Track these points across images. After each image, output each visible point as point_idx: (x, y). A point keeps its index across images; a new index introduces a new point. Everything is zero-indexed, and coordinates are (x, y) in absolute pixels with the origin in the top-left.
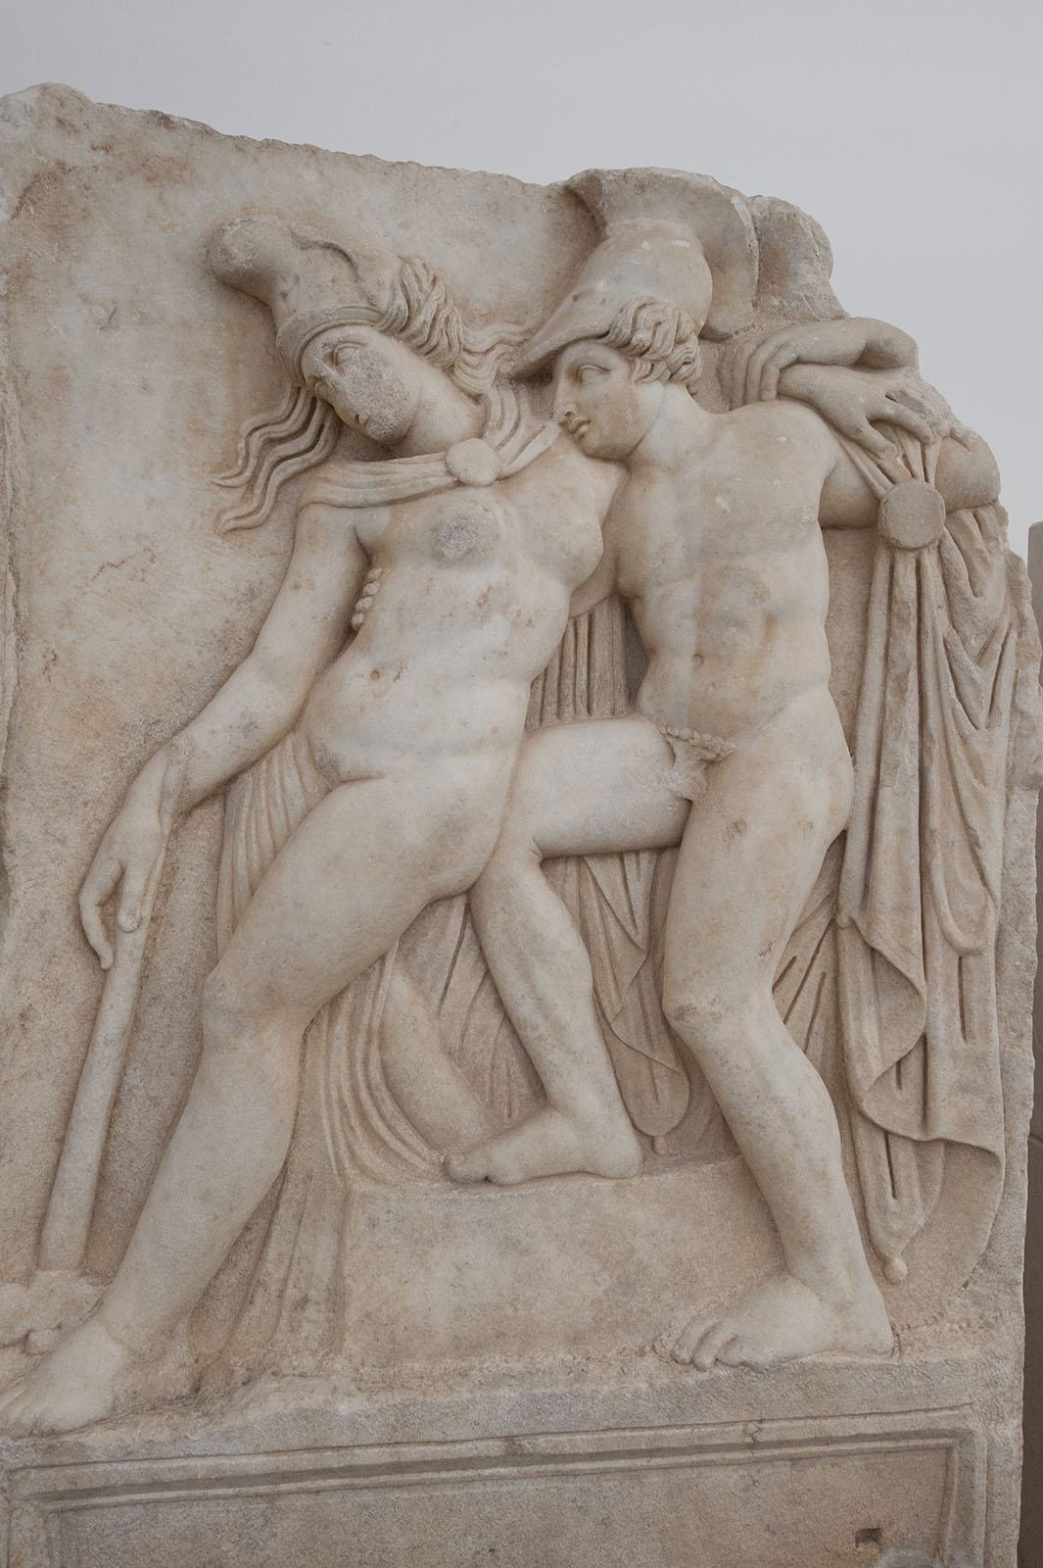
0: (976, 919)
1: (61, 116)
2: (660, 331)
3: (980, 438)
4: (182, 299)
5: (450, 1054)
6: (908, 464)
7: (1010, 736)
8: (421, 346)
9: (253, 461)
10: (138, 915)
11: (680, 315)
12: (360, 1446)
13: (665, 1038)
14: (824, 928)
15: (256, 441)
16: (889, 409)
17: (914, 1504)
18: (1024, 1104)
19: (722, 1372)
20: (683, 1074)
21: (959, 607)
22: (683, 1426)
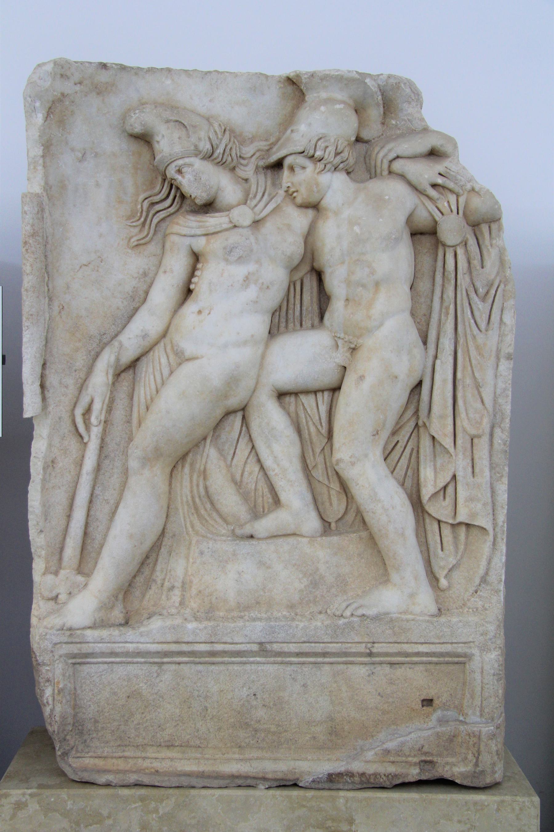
0: (479, 421)
1: (62, 73)
2: (328, 151)
3: (488, 190)
4: (113, 144)
5: (236, 483)
8: (219, 162)
9: (144, 214)
11: (338, 140)
13: (335, 477)
14: (413, 427)
15: (146, 204)
17: (449, 689)
18: (502, 507)
19: (355, 619)
20: (343, 493)
21: (474, 273)
22: (337, 643)
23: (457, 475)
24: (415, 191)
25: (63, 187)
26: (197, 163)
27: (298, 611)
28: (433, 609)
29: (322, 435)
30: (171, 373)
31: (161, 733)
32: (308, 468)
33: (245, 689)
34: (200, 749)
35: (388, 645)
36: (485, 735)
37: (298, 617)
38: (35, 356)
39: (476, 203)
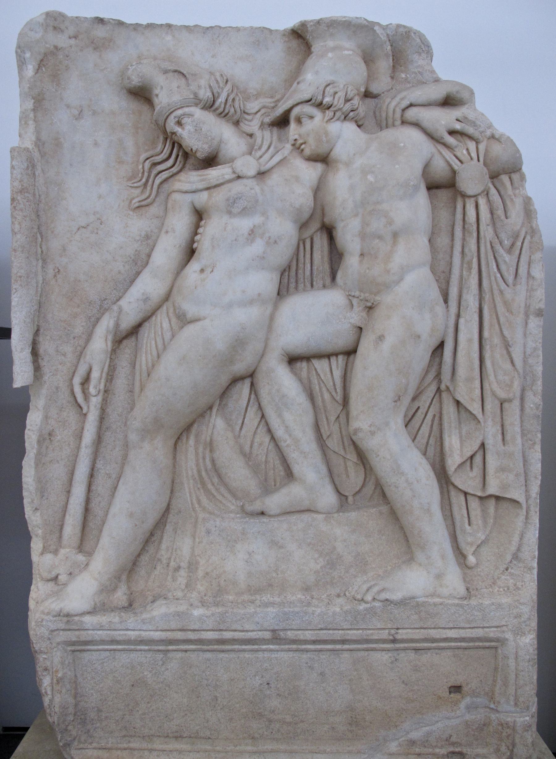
1: (55, 25)
2: (337, 96)
3: (508, 137)
4: (114, 102)
5: (244, 455)
6: (469, 154)
7: (527, 290)
8: (221, 113)
9: (146, 174)
10: (98, 389)
11: (348, 87)
12: (204, 630)
13: (352, 447)
14: (434, 392)
15: (147, 164)
16: (458, 126)
18: (536, 477)
19: (377, 604)
20: (361, 465)
21: (498, 224)
22: (358, 629)
23: (485, 443)
24: (431, 140)
25: (58, 144)
26: (198, 113)
27: (314, 593)
28: (462, 590)
29: (337, 402)
30: (173, 336)
31: (168, 723)
32: (322, 438)
33: (257, 677)
34: (210, 740)
35: (414, 631)
36: (520, 726)
37: (314, 601)
38: (25, 321)
39: (497, 149)
